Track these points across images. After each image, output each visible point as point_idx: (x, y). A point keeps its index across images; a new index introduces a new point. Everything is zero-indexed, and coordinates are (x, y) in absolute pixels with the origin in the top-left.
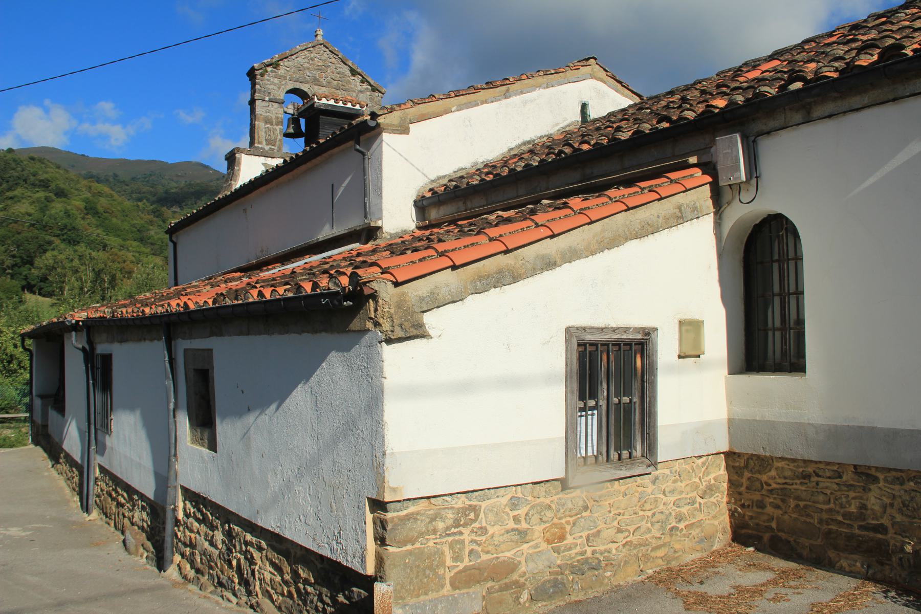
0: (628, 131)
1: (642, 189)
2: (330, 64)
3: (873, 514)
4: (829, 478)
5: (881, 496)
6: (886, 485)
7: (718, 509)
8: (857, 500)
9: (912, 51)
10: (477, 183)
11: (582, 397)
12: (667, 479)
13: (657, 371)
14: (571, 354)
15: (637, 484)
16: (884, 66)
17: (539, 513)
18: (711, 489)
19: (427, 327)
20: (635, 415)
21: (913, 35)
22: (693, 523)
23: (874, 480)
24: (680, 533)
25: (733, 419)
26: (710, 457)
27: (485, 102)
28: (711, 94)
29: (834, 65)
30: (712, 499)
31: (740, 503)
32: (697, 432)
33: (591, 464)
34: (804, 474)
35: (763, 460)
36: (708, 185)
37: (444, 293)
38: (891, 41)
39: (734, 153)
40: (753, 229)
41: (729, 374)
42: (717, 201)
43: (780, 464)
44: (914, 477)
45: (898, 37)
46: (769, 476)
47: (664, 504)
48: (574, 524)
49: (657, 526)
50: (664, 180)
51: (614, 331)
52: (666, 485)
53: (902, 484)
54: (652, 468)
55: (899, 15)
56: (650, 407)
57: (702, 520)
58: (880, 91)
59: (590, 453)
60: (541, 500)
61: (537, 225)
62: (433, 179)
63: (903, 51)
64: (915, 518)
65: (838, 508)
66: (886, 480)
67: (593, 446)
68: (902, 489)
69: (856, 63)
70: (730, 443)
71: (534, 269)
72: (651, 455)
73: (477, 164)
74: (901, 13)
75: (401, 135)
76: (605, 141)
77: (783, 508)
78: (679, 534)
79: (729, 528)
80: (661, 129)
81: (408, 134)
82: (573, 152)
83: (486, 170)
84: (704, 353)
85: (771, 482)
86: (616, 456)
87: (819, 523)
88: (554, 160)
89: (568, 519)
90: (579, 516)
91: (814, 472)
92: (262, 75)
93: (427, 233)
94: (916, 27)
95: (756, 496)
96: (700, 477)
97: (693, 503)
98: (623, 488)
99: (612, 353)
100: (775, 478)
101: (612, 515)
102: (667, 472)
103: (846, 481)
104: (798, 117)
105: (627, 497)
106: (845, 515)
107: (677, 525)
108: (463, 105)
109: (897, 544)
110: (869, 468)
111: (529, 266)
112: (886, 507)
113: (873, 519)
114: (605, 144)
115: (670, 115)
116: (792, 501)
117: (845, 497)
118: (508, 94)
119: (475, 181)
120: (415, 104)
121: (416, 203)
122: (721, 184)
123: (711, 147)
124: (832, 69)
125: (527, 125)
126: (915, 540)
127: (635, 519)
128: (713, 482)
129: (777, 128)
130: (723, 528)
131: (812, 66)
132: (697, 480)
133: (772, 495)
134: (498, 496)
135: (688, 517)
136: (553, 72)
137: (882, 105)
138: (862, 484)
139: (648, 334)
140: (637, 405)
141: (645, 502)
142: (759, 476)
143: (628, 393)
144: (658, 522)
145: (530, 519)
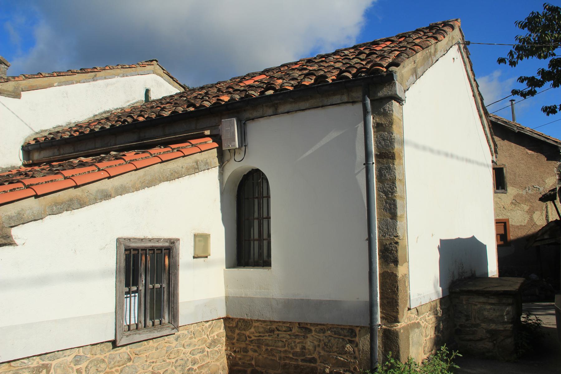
0: (169, 111)
1: (173, 149)
3: (309, 352)
4: (285, 331)
5: (313, 341)
6: (316, 334)
7: (219, 354)
8: (300, 344)
9: (331, 80)
10: (68, 137)
11: (127, 285)
12: (186, 337)
13: (179, 267)
14: (120, 256)
15: (165, 341)
16: (317, 87)
17: (96, 365)
18: (215, 342)
19: (14, 237)
20: (164, 295)
21: (332, 71)
22: (203, 365)
23: (309, 332)
24: (195, 372)
25: (229, 297)
26: (214, 321)
27: (79, 82)
28: (222, 92)
29: (291, 82)
30: (216, 349)
31: (233, 350)
32: (206, 306)
33: (133, 330)
34: (270, 329)
35: (246, 322)
36: (216, 149)
37: (28, 214)
38: (322, 73)
39: (232, 130)
40: (243, 177)
41: (226, 268)
42: (221, 159)
43: (256, 324)
44: (330, 328)
45: (326, 71)
46: (251, 332)
47: (184, 353)
48: (121, 371)
49: (179, 368)
50: (188, 144)
51: (150, 241)
52: (185, 341)
53: (324, 333)
54: (175, 330)
55: (330, 58)
56: (174, 290)
57: (209, 362)
58: (315, 101)
59: (132, 322)
60: (98, 356)
61: (99, 170)
62: (37, 131)
63: (327, 80)
64: (330, 352)
65: (290, 350)
66: (315, 331)
67: (135, 317)
68: (324, 336)
69: (302, 83)
70: (226, 312)
71: (96, 199)
72: (174, 322)
73: (71, 124)
74: (331, 57)
75: (14, 99)
76: (154, 116)
77: (259, 352)
78: (194, 373)
79: (226, 366)
80: (189, 111)
81: (20, 98)
82: (133, 121)
83: (75, 129)
84: (210, 255)
85: (251, 335)
86: (151, 323)
87: (279, 359)
88: (120, 126)
89: (117, 368)
90: (125, 365)
91: (276, 328)
93: (29, 169)
94: (336, 67)
95: (243, 345)
96: (208, 334)
97: (203, 352)
98: (156, 345)
99: (149, 255)
100: (254, 333)
101: (148, 363)
102: (186, 332)
103: (294, 333)
104: (270, 111)
105: (158, 350)
106: (293, 354)
107: (193, 367)
108: (62, 82)
109: (322, 368)
110: (307, 324)
111: (92, 197)
112: (316, 347)
113: (309, 355)
114: (154, 118)
115: (195, 103)
116: (263, 346)
117: (293, 343)
118: (95, 78)
119: (66, 136)
120: (26, 78)
121: (23, 148)
122: (224, 149)
123: (219, 125)
124: (290, 85)
125: (107, 100)
126: (331, 365)
127: (164, 365)
128: (216, 337)
129: (258, 117)
130: (223, 367)
131: (280, 81)
132: (206, 336)
133: (252, 343)
134: (65, 356)
135: (199, 361)
136: (128, 66)
137: (316, 109)
138: (303, 334)
139: (173, 243)
140: (165, 289)
141: (171, 353)
142: (243, 332)
143: (159, 281)
144: (180, 366)
145: (89, 370)
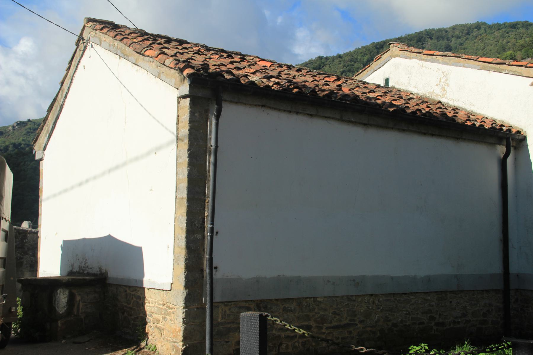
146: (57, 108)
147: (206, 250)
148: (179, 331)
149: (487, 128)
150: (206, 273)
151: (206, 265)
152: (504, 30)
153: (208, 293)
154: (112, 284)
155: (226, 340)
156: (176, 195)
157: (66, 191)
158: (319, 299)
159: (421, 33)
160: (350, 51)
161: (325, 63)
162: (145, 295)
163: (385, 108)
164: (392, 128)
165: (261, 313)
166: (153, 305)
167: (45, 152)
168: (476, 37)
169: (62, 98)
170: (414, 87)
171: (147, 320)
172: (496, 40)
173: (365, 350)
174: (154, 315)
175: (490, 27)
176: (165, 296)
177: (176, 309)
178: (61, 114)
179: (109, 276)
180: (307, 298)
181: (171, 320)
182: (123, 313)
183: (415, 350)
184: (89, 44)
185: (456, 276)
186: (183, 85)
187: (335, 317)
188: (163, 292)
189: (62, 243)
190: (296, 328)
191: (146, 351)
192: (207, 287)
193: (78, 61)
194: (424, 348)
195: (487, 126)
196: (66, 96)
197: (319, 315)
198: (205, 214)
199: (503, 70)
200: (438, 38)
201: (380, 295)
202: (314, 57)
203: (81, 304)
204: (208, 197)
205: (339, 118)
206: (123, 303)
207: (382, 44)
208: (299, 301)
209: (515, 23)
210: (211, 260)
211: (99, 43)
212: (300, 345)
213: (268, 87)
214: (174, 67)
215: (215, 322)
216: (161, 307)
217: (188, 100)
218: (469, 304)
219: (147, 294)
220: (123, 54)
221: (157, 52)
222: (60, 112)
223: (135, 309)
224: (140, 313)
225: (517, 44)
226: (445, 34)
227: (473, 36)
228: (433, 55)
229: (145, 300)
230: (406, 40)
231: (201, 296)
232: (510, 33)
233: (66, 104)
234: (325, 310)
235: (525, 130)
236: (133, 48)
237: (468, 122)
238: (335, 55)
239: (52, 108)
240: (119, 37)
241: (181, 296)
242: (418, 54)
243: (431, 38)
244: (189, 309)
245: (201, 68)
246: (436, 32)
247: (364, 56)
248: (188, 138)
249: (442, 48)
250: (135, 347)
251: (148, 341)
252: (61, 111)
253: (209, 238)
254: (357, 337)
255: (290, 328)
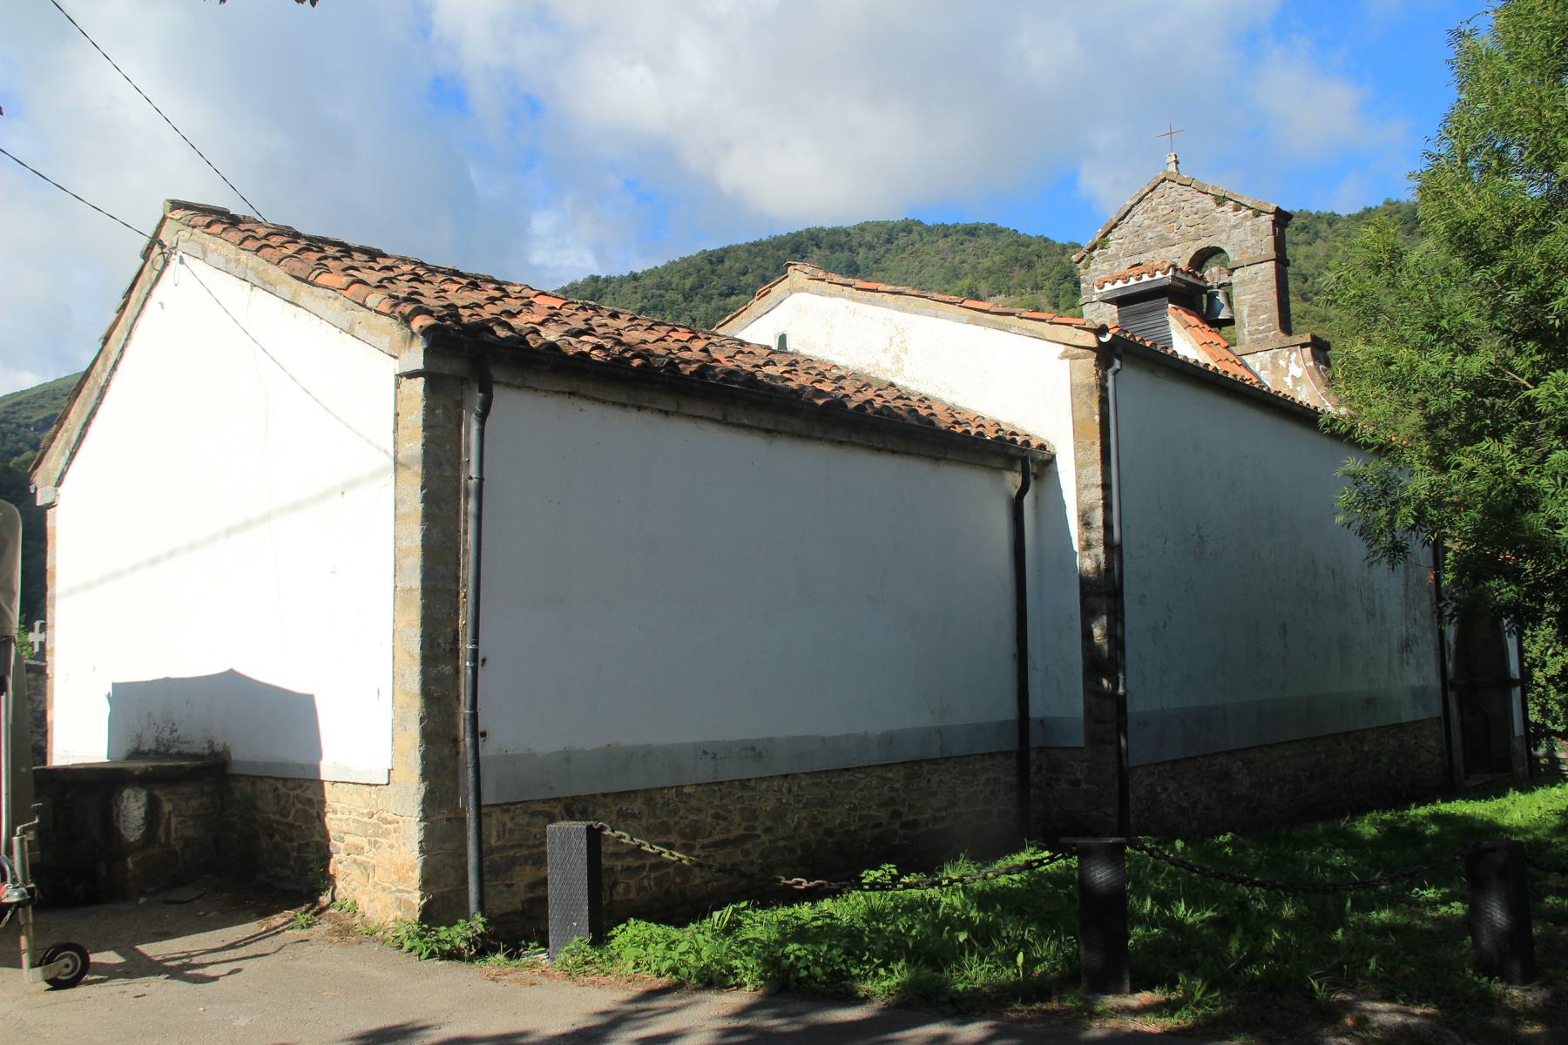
2: (1183, 204)
92: (1087, 266)
146: (90, 394)
147: (462, 697)
148: (412, 869)
149: (988, 438)
150: (465, 745)
151: (464, 729)
152: (955, 237)
153: (471, 787)
154: (240, 775)
155: (508, 882)
156: (395, 582)
157: (117, 575)
158: (686, 790)
159: (799, 234)
160: (656, 268)
161: (605, 290)
162: (323, 796)
163: (808, 399)
164: (820, 439)
165: (589, 823)
166: (346, 816)
167: (61, 490)
168: (904, 250)
169: (104, 370)
170: (838, 354)
171: (331, 849)
172: (941, 256)
173: (805, 884)
174: (348, 838)
175: (929, 230)
176: (374, 796)
177: (401, 822)
178: (102, 406)
179: (233, 758)
180: (665, 788)
181: (391, 847)
182: (271, 837)
183: (872, 878)
184: (173, 256)
185: (939, 730)
186: (409, 351)
187: (718, 824)
188: (368, 789)
189: (109, 689)
190: (665, 850)
191: (334, 914)
192: (467, 776)
193: (146, 292)
194: (890, 872)
195: (990, 435)
196: (115, 367)
197: (687, 822)
198: (460, 622)
199: (1010, 326)
200: (832, 247)
201: (802, 776)
202: (580, 277)
203: (174, 821)
204: (465, 586)
205: (721, 418)
206: (271, 815)
207: (722, 254)
208: (649, 795)
209: (974, 226)
210: (474, 717)
211: (200, 255)
212: (652, 883)
213: (582, 354)
214: (389, 312)
215: (485, 847)
216: (366, 819)
217: (420, 382)
218: (959, 782)
219: (330, 794)
220: (262, 279)
221: (345, 280)
222: (99, 401)
223: (301, 827)
224: (313, 835)
225: (979, 266)
226: (847, 239)
227: (898, 245)
228: (877, 291)
229: (325, 807)
230: (770, 247)
231: (456, 793)
232: (966, 244)
233: (114, 383)
234: (699, 810)
235: (1052, 442)
236: (286, 269)
237: (956, 426)
238: (626, 274)
239: (80, 392)
240: (250, 244)
241: (415, 794)
242: (845, 288)
243: (819, 247)
244: (431, 823)
245: (448, 315)
246: (828, 234)
247: (684, 279)
248: (421, 461)
249: (840, 266)
250: (308, 905)
251: (336, 893)
252: (102, 400)
253: (469, 672)
254: (760, 861)
255: (651, 850)
